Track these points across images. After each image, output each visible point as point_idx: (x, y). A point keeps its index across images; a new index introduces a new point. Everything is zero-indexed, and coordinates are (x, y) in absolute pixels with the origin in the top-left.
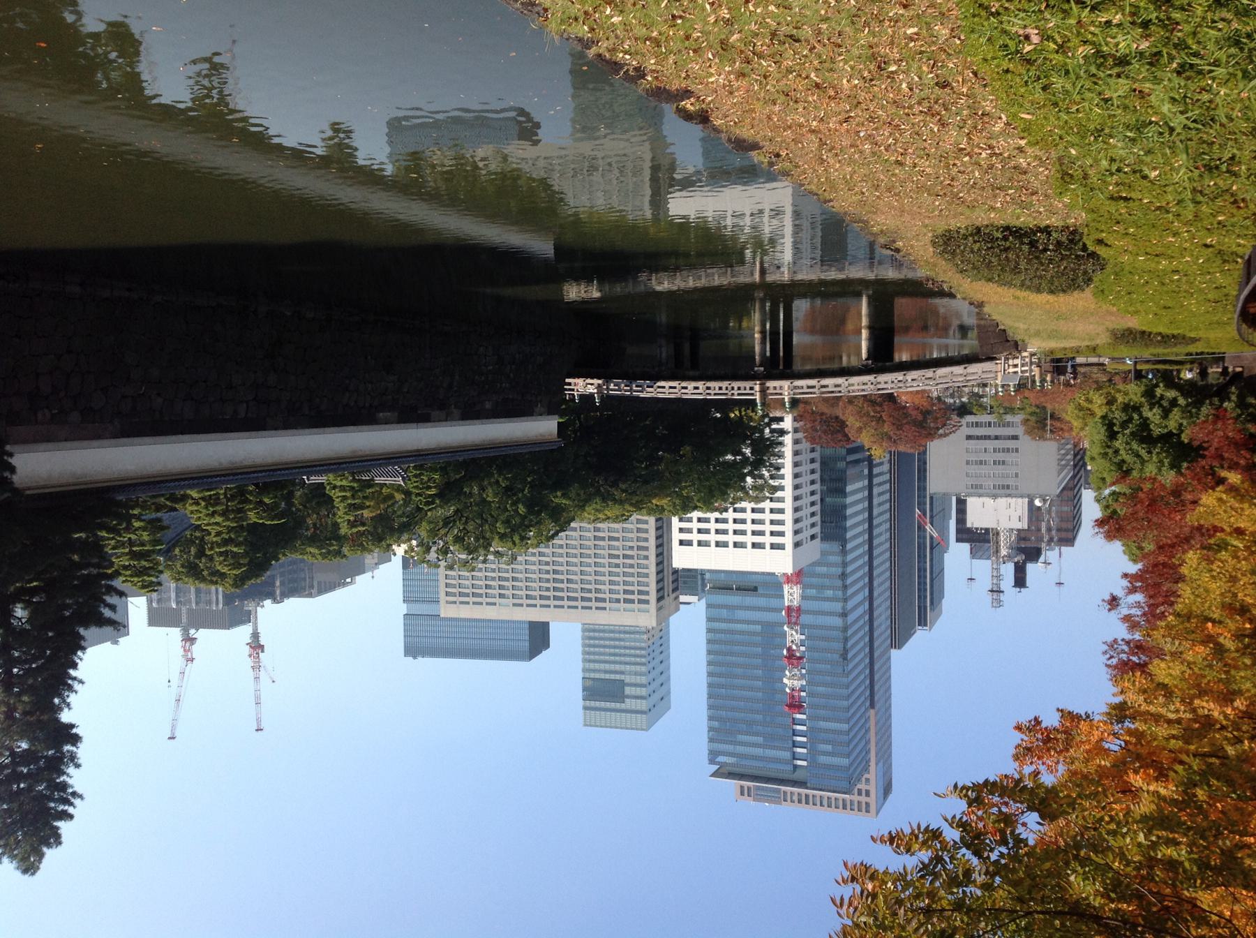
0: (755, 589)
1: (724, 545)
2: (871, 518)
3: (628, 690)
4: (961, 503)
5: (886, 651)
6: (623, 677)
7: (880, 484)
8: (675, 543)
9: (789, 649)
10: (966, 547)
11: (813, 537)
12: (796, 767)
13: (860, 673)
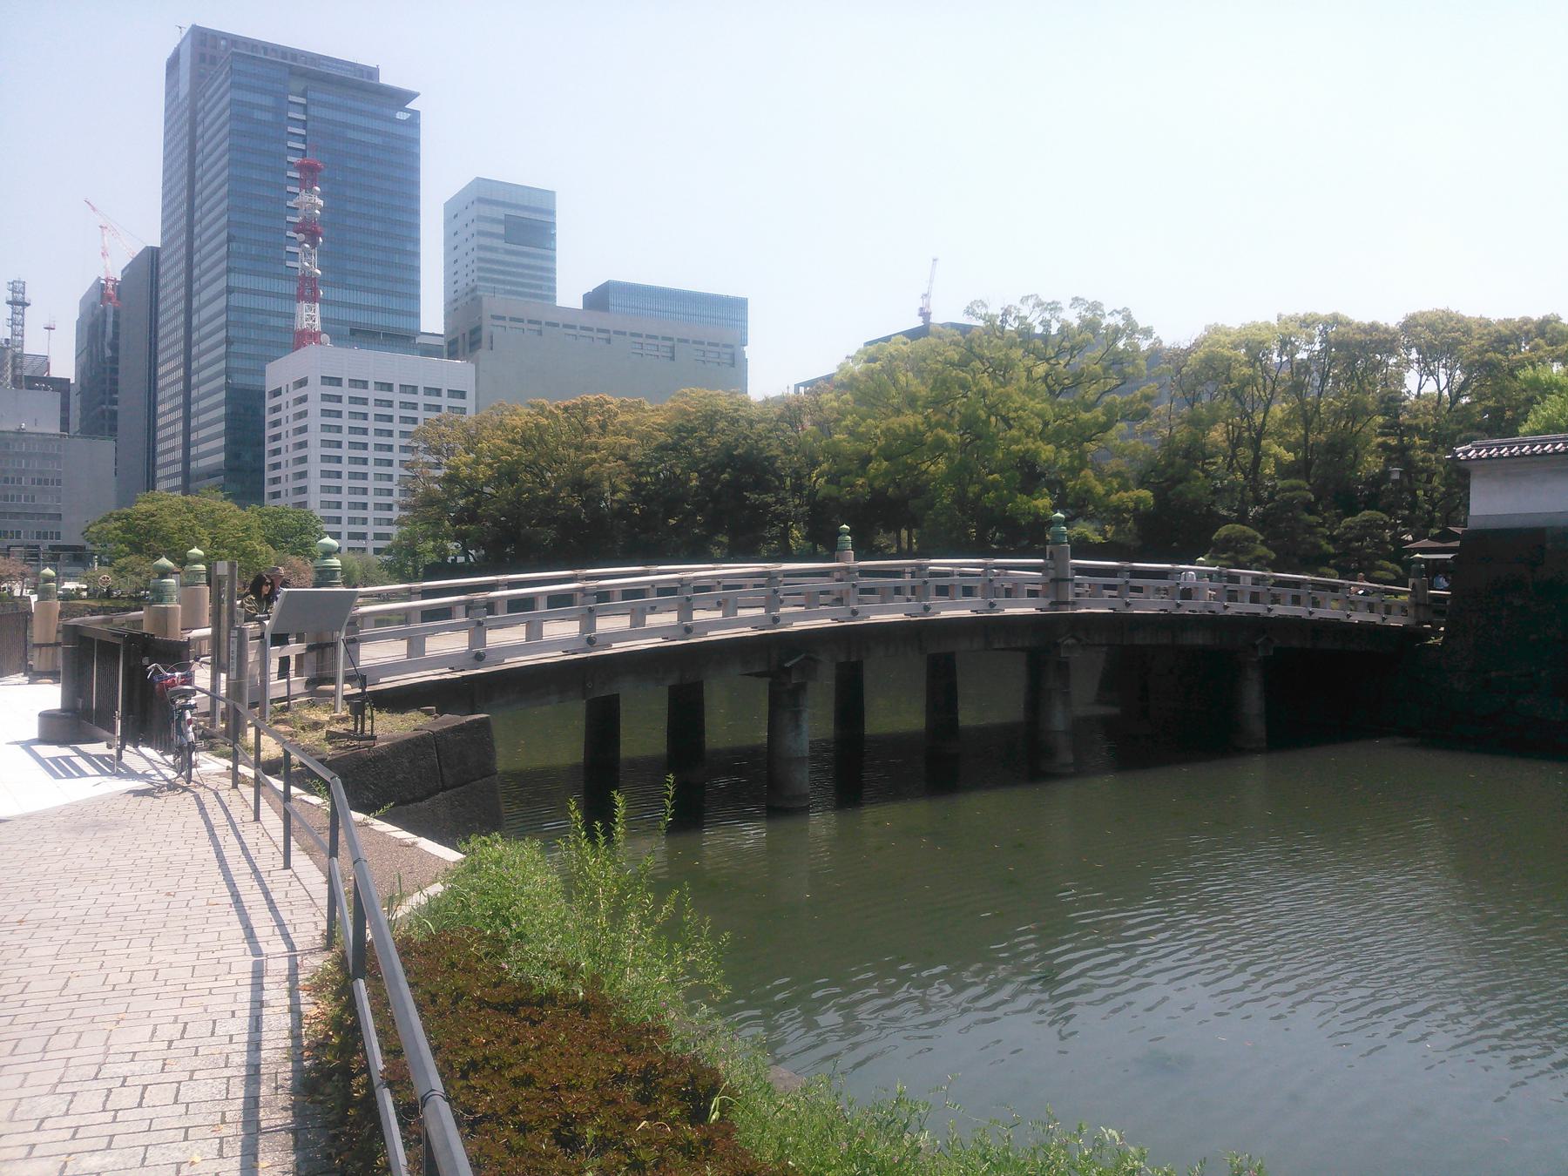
0: (353, 332)
1: (429, 391)
2: (187, 404)
3: (500, 229)
4: (65, 423)
5: (165, 245)
6: (508, 246)
7: (173, 462)
8: (471, 395)
9: (314, 244)
10: (55, 373)
11: (277, 393)
12: (304, 95)
13: (207, 228)
